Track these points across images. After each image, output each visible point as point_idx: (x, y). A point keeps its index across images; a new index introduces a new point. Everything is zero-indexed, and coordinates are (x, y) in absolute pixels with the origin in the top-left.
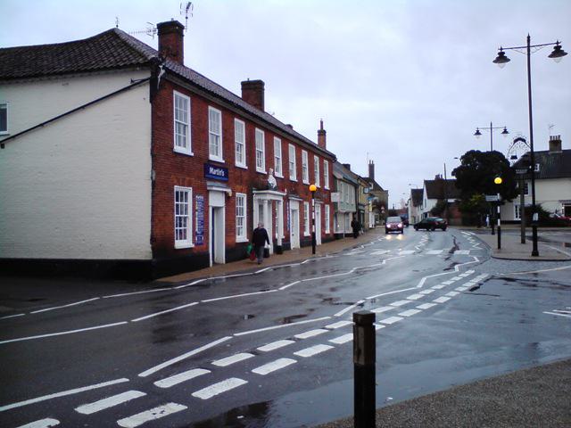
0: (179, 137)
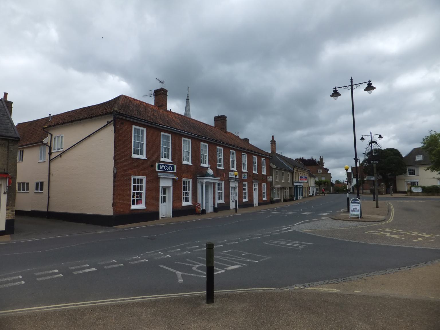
0: (232, 165)
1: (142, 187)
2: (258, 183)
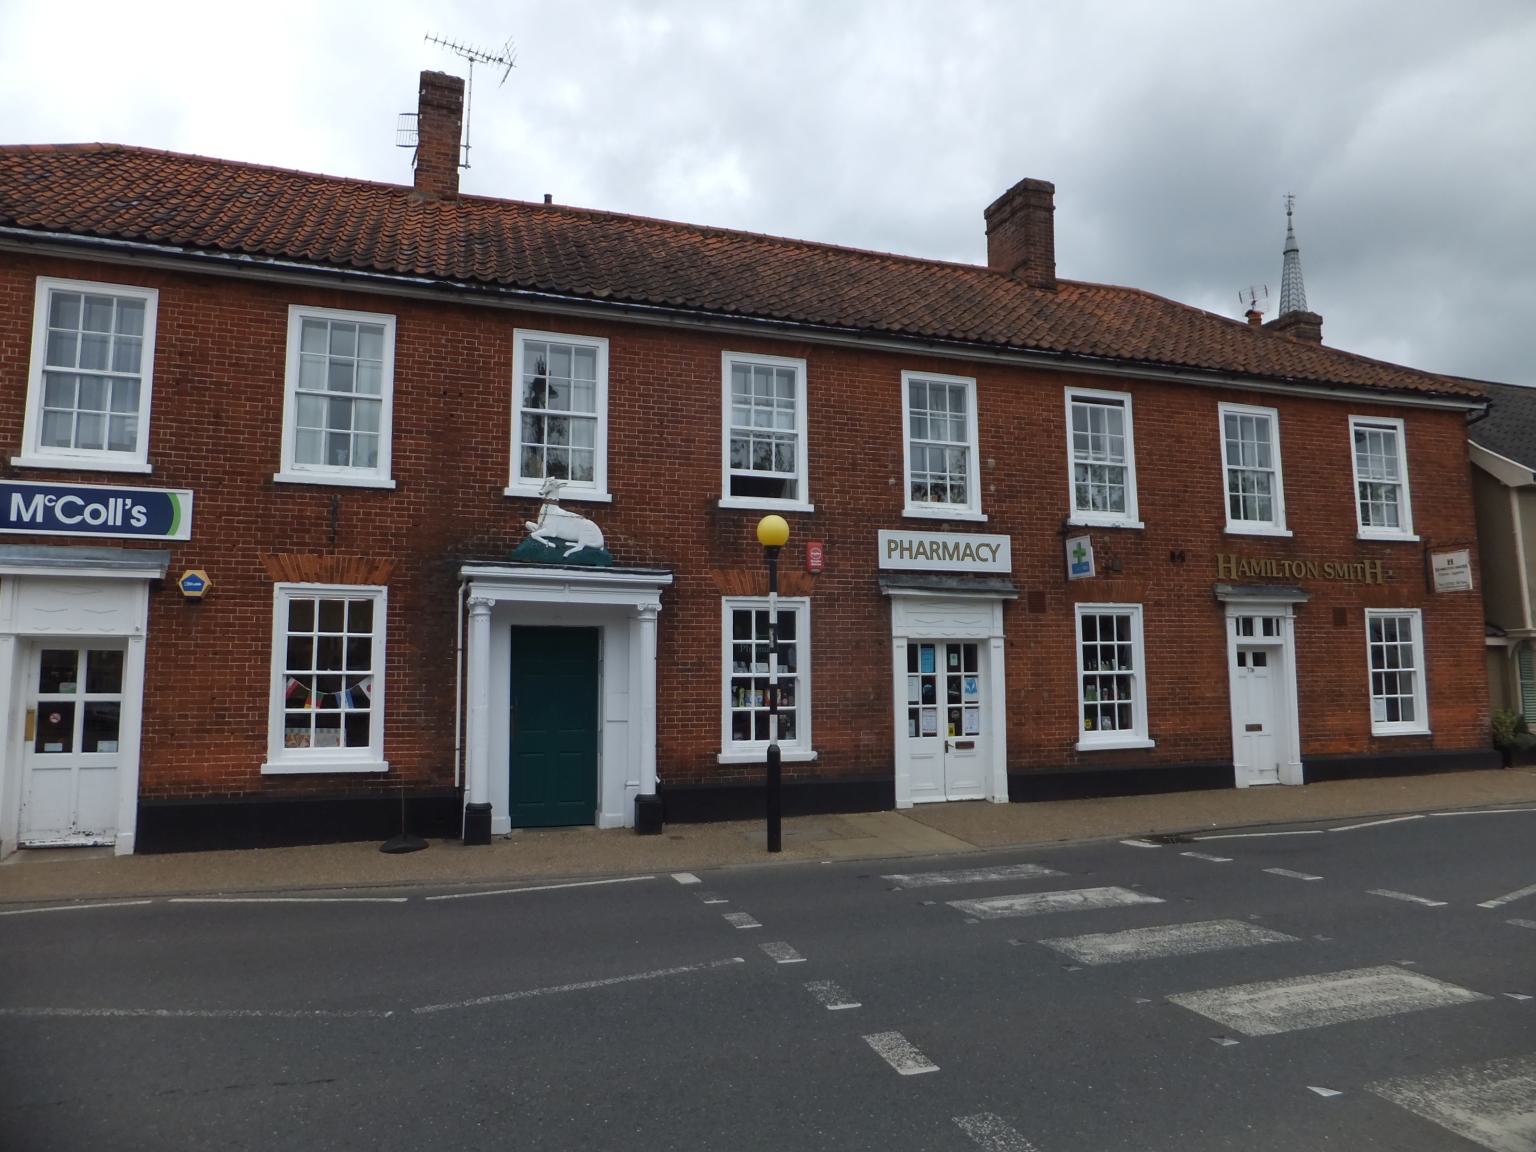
1: (1408, 652)
2: (1296, 607)
